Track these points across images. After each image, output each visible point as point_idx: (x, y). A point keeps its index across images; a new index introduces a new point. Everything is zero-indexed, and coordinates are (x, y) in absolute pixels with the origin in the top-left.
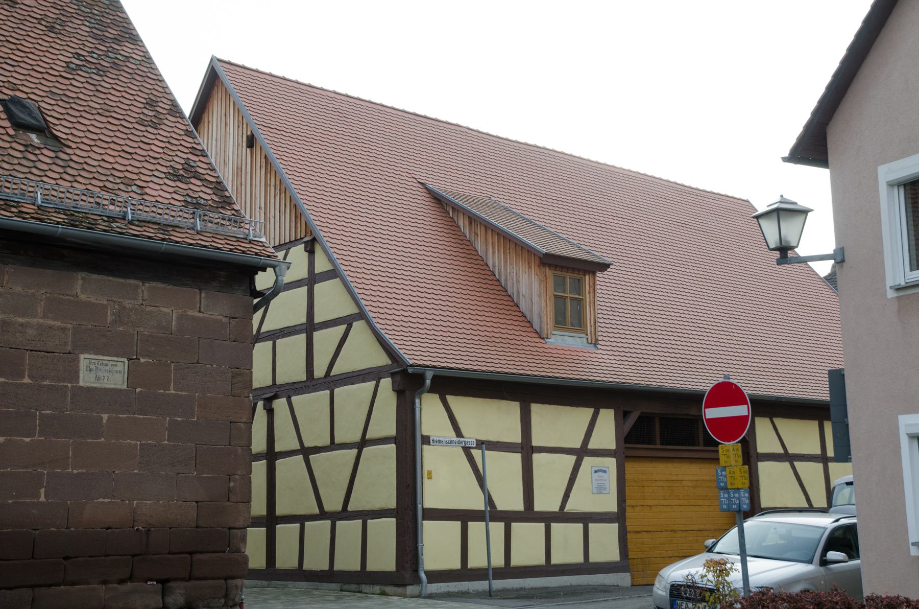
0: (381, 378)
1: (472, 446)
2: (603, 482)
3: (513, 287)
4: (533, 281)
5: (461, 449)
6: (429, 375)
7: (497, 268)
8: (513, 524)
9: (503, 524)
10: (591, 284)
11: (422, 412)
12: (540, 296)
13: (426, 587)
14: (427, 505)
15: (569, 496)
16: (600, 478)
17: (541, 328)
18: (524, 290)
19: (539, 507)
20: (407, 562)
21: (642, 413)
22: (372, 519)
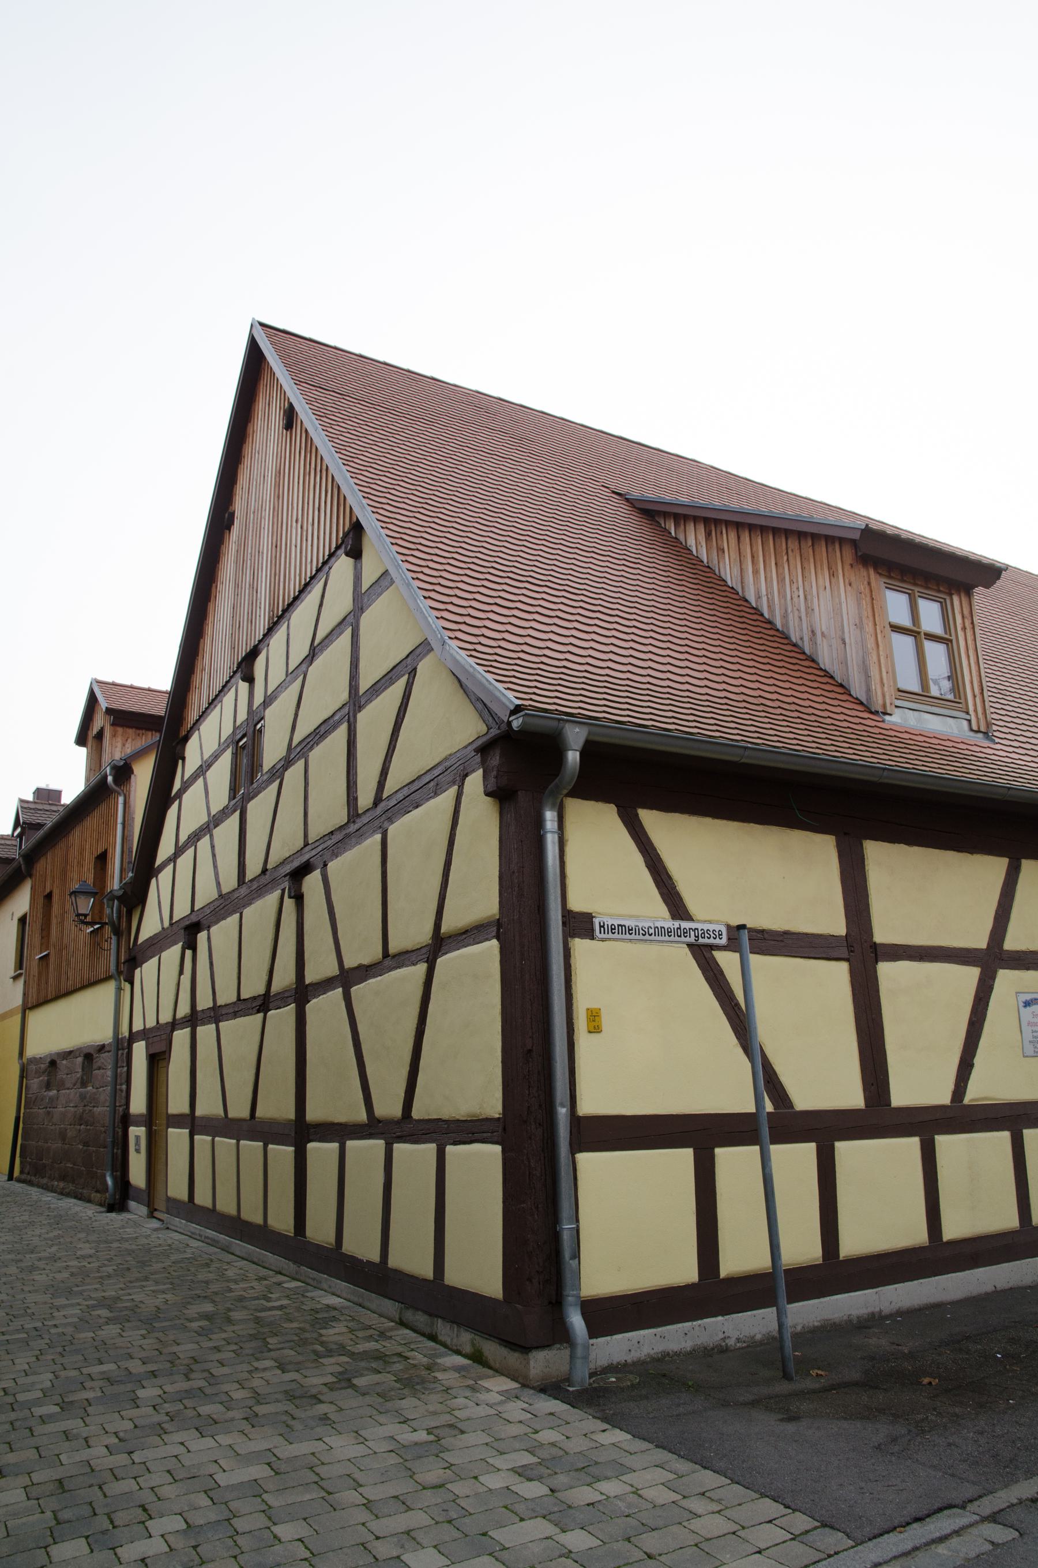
0: (466, 775)
1: (717, 941)
5: (687, 950)
6: (575, 737)
7: (764, 599)
8: (839, 1145)
10: (966, 612)
11: (569, 850)
12: (860, 626)
13: (587, 1347)
14: (587, 1107)
15: (972, 1066)
17: (868, 690)
18: (823, 620)
19: (901, 1095)
20: (530, 1280)
22: (455, 1143)
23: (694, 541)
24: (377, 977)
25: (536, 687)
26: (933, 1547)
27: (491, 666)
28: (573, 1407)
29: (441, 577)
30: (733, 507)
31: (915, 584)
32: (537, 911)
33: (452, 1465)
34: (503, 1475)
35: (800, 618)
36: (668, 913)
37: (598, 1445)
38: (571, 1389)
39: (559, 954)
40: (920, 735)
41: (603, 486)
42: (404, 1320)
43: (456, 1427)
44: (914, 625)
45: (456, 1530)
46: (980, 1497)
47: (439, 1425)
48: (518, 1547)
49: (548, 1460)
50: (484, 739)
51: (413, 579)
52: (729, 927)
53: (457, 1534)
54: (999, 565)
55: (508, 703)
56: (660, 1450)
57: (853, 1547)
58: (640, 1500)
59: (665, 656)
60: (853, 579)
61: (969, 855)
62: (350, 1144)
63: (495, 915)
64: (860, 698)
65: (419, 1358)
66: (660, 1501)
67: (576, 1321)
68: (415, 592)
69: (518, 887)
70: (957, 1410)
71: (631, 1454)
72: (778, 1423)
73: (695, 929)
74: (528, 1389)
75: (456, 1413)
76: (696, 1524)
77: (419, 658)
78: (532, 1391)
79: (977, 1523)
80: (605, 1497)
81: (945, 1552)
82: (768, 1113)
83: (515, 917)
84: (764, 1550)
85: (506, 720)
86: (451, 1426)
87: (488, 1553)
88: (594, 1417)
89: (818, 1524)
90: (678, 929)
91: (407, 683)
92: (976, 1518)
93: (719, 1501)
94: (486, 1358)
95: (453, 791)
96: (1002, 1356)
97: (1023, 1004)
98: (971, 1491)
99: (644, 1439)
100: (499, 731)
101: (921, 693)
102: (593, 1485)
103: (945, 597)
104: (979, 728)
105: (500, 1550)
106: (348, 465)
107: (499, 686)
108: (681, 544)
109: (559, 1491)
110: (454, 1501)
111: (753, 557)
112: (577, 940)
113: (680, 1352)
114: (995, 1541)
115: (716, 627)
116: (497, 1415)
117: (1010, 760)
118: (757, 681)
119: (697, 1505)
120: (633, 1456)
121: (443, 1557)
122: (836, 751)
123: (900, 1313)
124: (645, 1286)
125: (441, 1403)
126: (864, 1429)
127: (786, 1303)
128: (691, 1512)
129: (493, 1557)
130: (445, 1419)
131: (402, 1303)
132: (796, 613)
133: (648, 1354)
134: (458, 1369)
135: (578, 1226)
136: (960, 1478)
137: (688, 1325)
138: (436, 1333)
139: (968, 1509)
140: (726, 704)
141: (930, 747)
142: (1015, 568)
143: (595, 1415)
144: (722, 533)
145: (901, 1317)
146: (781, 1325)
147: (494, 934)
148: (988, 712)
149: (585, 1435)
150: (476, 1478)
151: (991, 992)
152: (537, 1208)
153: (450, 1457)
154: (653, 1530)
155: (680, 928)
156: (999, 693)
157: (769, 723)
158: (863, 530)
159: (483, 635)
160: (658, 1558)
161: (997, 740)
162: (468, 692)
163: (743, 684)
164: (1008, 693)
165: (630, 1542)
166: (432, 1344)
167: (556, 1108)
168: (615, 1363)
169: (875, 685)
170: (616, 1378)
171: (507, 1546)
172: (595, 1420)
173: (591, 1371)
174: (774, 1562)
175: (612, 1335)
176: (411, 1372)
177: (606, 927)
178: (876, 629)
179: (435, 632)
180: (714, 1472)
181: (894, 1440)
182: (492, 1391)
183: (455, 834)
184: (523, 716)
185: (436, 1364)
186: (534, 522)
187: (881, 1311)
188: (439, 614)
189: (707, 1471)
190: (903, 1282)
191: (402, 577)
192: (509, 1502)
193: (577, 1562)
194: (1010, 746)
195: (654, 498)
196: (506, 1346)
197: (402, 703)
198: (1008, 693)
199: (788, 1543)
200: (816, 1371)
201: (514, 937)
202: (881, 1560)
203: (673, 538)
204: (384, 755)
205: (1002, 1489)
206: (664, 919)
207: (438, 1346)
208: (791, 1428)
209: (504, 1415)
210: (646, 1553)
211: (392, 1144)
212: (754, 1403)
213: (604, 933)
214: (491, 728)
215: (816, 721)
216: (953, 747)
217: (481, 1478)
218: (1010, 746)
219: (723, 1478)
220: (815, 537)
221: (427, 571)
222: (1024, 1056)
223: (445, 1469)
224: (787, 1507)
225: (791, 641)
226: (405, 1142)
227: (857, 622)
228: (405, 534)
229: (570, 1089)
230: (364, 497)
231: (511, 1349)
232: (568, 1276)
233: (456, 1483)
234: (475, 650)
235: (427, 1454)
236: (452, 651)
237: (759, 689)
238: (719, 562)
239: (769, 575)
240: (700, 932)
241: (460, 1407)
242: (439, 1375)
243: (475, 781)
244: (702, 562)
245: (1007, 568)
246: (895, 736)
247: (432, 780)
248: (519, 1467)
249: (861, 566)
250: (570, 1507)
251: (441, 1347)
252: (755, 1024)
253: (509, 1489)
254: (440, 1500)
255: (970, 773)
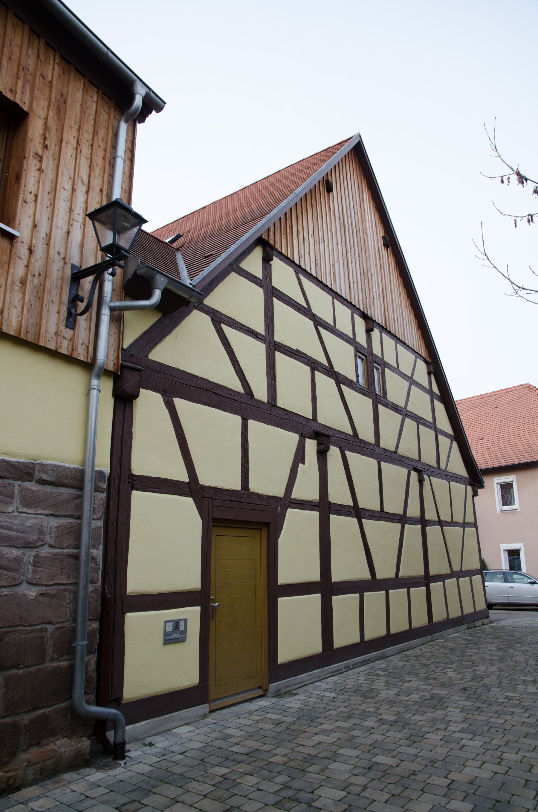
62: (446, 581)
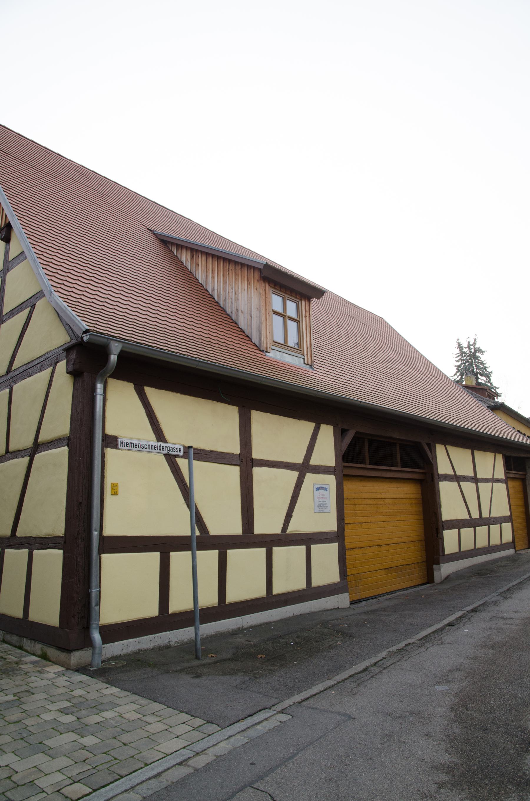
0: (58, 362)
1: (178, 453)
2: (324, 500)
3: (232, 306)
4: (253, 296)
5: (163, 457)
6: (116, 348)
7: (216, 291)
8: (229, 551)
9: (216, 552)
10: (307, 309)
12: (259, 309)
13: (101, 649)
14: (108, 531)
15: (291, 516)
16: (321, 496)
17: (260, 340)
18: (242, 305)
19: (259, 529)
20: (73, 617)
21: (357, 433)
22: (39, 549)
23: (185, 259)
24: (2, 463)
25: (98, 321)
26: (255, 726)
27: (75, 308)
28: (92, 678)
29: (53, 259)
30: (191, 241)
31: (286, 293)
32: (89, 434)
33: (26, 711)
34: (53, 713)
35: (232, 302)
36: (155, 439)
37: (103, 695)
38: (91, 669)
39: (99, 455)
40: (275, 361)
41: (142, 225)
42: (5, 640)
43: (30, 691)
44: (284, 312)
45: (25, 743)
46: (278, 703)
47: (20, 691)
48: (58, 747)
49: (77, 704)
50: (69, 345)
51: (38, 258)
52: (184, 447)
53: (26, 744)
54: (324, 289)
55: (82, 328)
56: (134, 695)
57: (220, 730)
58: (122, 719)
59: (165, 313)
60: (258, 287)
61: (298, 420)
63: (67, 434)
64: (256, 343)
65: (12, 658)
66: (132, 719)
67: (96, 636)
68: (37, 264)
69: (81, 420)
70: (272, 668)
71: (119, 698)
72: (191, 679)
73: (168, 447)
74: (70, 671)
75: (30, 685)
76: (148, 728)
77: (37, 299)
78: (71, 672)
79: (275, 714)
80: (105, 719)
81: (260, 728)
82: (196, 536)
83: (78, 436)
84: (180, 736)
85: (80, 336)
86: (27, 691)
87: (41, 752)
88: (102, 682)
89: (206, 722)
90: (159, 446)
91: (30, 311)
92: (275, 712)
93: (160, 716)
94: (49, 656)
95: (50, 369)
96: (294, 644)
97: (316, 489)
98: (274, 701)
99: (126, 691)
100: (76, 341)
101: (298, 348)
102: (99, 714)
103: (299, 301)
104: (308, 363)
105: (48, 750)
106: (6, 192)
107: (79, 318)
108: (179, 259)
109: (82, 718)
110: (25, 728)
111: (212, 270)
112: (109, 449)
113: (148, 649)
114: (282, 721)
115: (191, 302)
116: (52, 684)
117: (320, 379)
118: (208, 330)
119: (149, 719)
120: (120, 699)
121: (17, 757)
122: (242, 367)
123: (251, 627)
124: (132, 618)
125: (22, 680)
126: (231, 679)
127: (199, 624)
128: (147, 722)
129: (44, 753)
130: (26, 688)
131: (5, 631)
132: (230, 300)
133: (132, 651)
134: (33, 663)
135: (100, 590)
136: (270, 697)
137: (152, 636)
138: (22, 645)
139: (272, 709)
140: (192, 339)
141: (285, 369)
142: (336, 295)
143: (103, 681)
144: (199, 256)
145: (251, 629)
146: (196, 634)
147: (66, 443)
148: (312, 356)
149: (97, 691)
150: (38, 716)
151: (303, 483)
152: (80, 581)
153: (25, 707)
154: (127, 732)
155: (161, 446)
156: (318, 348)
157: (212, 351)
158: (265, 265)
159: (72, 292)
160: (128, 745)
161: (315, 369)
162: (62, 320)
163: (202, 331)
164: (322, 348)
165: (115, 739)
166: (20, 651)
167: (92, 532)
168: (115, 655)
169: (263, 338)
170: (115, 663)
171: (52, 747)
172: (103, 683)
173: (103, 660)
174: (184, 741)
175: (114, 642)
176: (7, 666)
177: (124, 443)
178: (266, 312)
179: (47, 287)
180: (159, 703)
181: (243, 683)
182: (50, 672)
183: (49, 392)
184: (89, 335)
185: (21, 661)
186: (105, 237)
187: (243, 627)
188: (50, 278)
189: (156, 703)
190: (254, 613)
191: (31, 256)
192: (55, 726)
193: (88, 751)
194: (321, 372)
195: (168, 235)
196: (59, 650)
197: (26, 322)
198: (322, 348)
199: (191, 732)
200: (211, 655)
201: (76, 445)
202: (232, 735)
203: (174, 255)
204: (14, 347)
205: (287, 699)
206: (153, 441)
207: (23, 652)
208: (197, 681)
209: (56, 684)
210: (123, 743)
211: (5, 549)
212: (181, 671)
213: (123, 446)
214: (73, 339)
215: (234, 352)
216: (296, 370)
217: (41, 716)
218: (321, 372)
219: (164, 706)
220: (242, 265)
221: (45, 254)
222: (314, 513)
223: (22, 713)
224: (192, 716)
225: (227, 313)
226: (11, 548)
227: (258, 307)
228: (35, 233)
229: (100, 522)
230: (14, 211)
231: (62, 651)
232: (93, 615)
233: (27, 719)
234: (67, 299)
235: (12, 706)
236: (55, 298)
237: (209, 334)
238: (196, 271)
239: (219, 280)
240: (170, 449)
241: (33, 682)
242: (22, 666)
243: (62, 366)
244: (188, 269)
245: (327, 291)
246: (270, 363)
247: (39, 363)
248: (61, 709)
249: (262, 281)
250: (86, 725)
251: (25, 652)
252: (193, 493)
253: (55, 720)
254: (18, 729)
255: (302, 383)
